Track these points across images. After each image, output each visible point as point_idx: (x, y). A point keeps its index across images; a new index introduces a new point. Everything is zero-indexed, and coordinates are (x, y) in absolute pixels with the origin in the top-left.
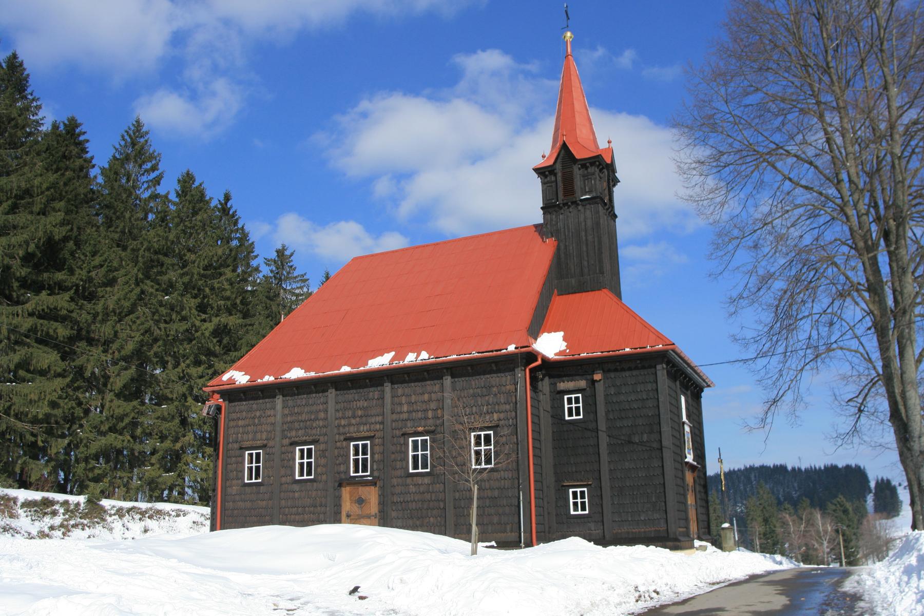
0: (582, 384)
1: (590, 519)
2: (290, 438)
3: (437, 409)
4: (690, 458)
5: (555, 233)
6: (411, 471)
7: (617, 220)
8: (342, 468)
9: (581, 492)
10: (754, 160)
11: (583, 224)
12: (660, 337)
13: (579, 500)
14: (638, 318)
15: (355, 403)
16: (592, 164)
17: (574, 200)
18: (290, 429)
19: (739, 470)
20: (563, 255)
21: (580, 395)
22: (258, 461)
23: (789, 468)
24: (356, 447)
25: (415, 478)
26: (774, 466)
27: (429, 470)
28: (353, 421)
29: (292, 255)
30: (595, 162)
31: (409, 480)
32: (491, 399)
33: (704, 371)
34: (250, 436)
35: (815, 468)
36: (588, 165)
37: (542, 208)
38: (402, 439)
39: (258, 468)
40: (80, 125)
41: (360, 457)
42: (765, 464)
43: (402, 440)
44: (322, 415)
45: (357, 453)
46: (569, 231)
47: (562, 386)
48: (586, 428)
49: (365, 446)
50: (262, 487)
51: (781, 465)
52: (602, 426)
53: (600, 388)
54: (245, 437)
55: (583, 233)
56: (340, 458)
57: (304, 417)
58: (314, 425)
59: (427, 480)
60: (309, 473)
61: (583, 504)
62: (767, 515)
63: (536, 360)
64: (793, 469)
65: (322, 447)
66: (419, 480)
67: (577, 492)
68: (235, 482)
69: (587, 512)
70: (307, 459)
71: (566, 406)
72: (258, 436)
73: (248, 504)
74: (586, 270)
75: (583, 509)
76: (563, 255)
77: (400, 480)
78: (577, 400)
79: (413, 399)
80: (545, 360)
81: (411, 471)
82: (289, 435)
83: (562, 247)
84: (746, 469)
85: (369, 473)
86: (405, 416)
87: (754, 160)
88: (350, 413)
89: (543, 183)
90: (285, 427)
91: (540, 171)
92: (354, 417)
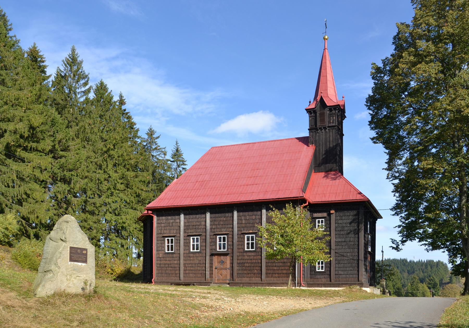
0: (325, 215)
1: (325, 274)
4: (370, 250)
5: (315, 142)
6: (246, 249)
7: (344, 137)
8: (214, 247)
11: (328, 139)
14: (352, 186)
16: (335, 109)
17: (325, 126)
18: (188, 229)
20: (318, 154)
21: (324, 220)
22: (172, 242)
23: (408, 261)
24: (220, 238)
25: (248, 253)
26: (400, 259)
27: (254, 250)
28: (218, 227)
29: (158, 137)
30: (336, 108)
31: (245, 254)
33: (380, 212)
36: (333, 109)
37: (309, 129)
38: (214, 236)
39: (172, 246)
41: (222, 242)
42: (396, 258)
43: (242, 236)
45: (220, 241)
46: (321, 142)
47: (315, 215)
49: (224, 238)
50: (174, 255)
53: (333, 217)
54: (165, 231)
55: (328, 143)
56: (212, 243)
57: (194, 224)
58: (200, 228)
59: (253, 254)
60: (172, 250)
61: (322, 267)
62: (394, 284)
63: (306, 203)
64: (410, 261)
65: (177, 238)
66: (250, 254)
69: (324, 270)
72: (172, 231)
75: (322, 269)
76: (318, 154)
78: (322, 222)
79: (248, 217)
81: (246, 249)
82: (187, 231)
83: (318, 149)
86: (243, 225)
89: (310, 117)
91: (308, 111)
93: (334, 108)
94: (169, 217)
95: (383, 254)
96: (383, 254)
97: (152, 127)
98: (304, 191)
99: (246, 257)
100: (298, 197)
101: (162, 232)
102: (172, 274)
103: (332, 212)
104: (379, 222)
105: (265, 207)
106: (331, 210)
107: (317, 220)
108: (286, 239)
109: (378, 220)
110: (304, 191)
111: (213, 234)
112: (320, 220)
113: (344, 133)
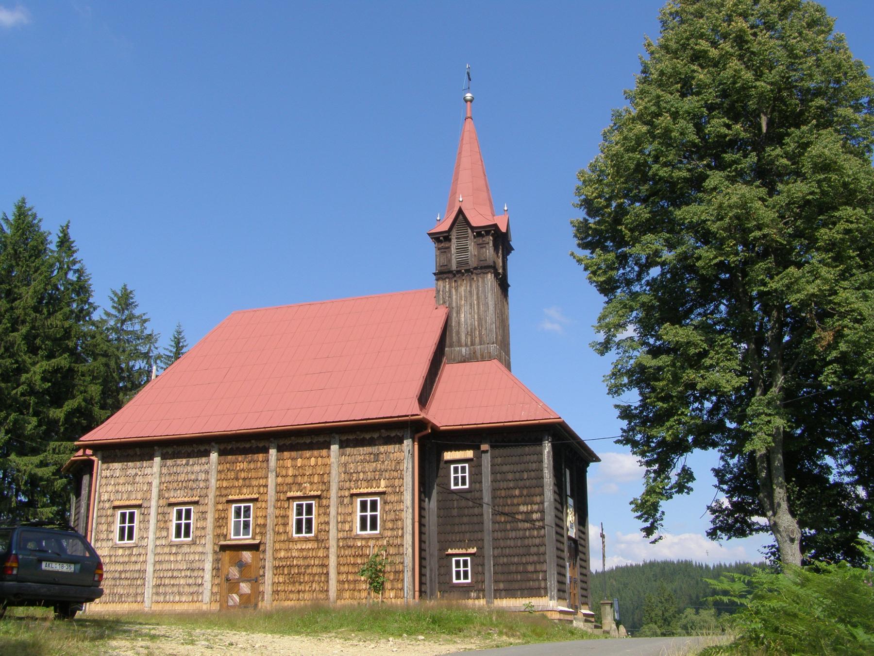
0: (469, 454)
2: (168, 499)
3: (323, 474)
9: (464, 560)
10: (176, 578)
12: (545, 409)
13: (462, 569)
15: (238, 464)
17: (468, 268)
18: (168, 489)
19: (638, 566)
28: (236, 484)
32: (379, 465)
33: (590, 445)
34: (125, 497)
35: (725, 565)
40: (727, 497)
44: (202, 476)
48: (472, 497)
51: (686, 561)
52: (487, 498)
53: (486, 459)
59: (309, 545)
61: (466, 573)
63: (426, 429)
67: (458, 467)
68: (104, 544)
70: (185, 520)
71: (452, 475)
73: (119, 568)
74: (477, 340)
77: (282, 545)
80: (434, 428)
82: (166, 496)
84: (645, 565)
85: (250, 536)
87: (176, 578)
88: (232, 475)
90: (164, 487)
92: (237, 479)
93: (485, 231)
94: (131, 464)
95: (603, 542)
96: (603, 542)
97: (182, 328)
98: (424, 398)
99: (295, 554)
100: (407, 416)
101: (112, 499)
102: (128, 595)
103: (485, 447)
104: (592, 470)
105: (338, 440)
106: (481, 443)
107: (452, 466)
108: (818, 281)
109: (591, 464)
110: (424, 398)
111: (224, 499)
112: (460, 466)
113: (509, 282)
